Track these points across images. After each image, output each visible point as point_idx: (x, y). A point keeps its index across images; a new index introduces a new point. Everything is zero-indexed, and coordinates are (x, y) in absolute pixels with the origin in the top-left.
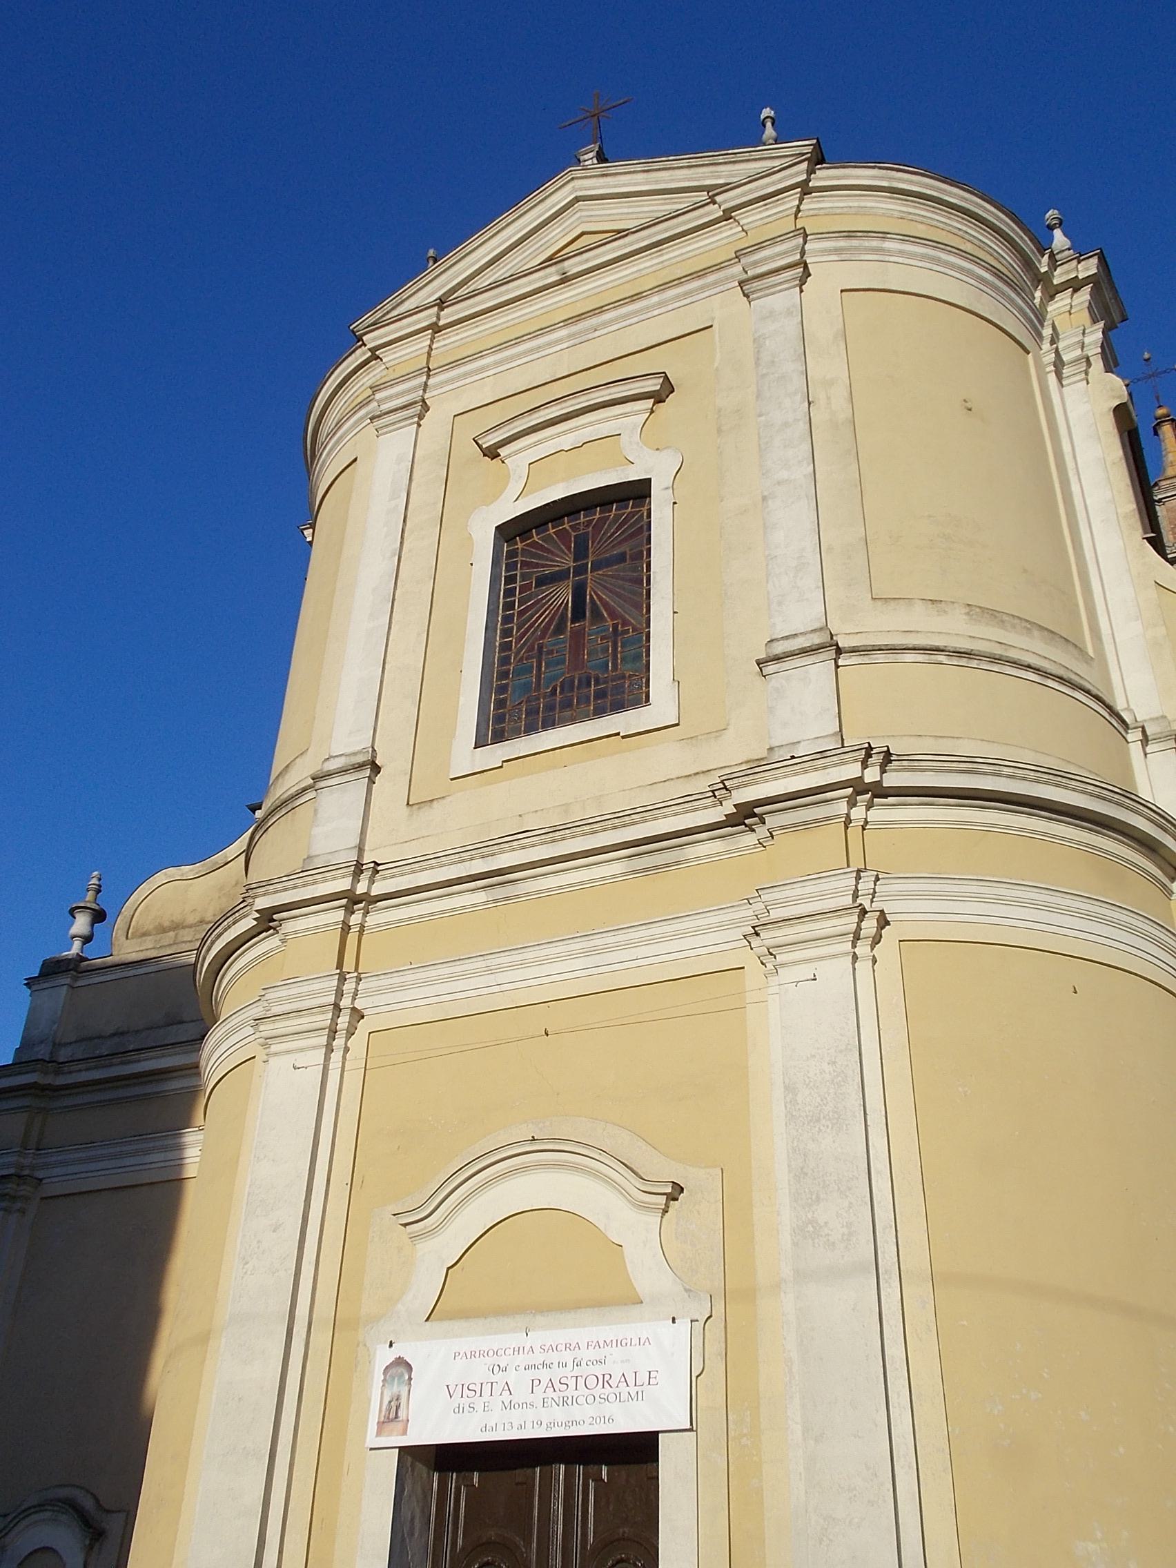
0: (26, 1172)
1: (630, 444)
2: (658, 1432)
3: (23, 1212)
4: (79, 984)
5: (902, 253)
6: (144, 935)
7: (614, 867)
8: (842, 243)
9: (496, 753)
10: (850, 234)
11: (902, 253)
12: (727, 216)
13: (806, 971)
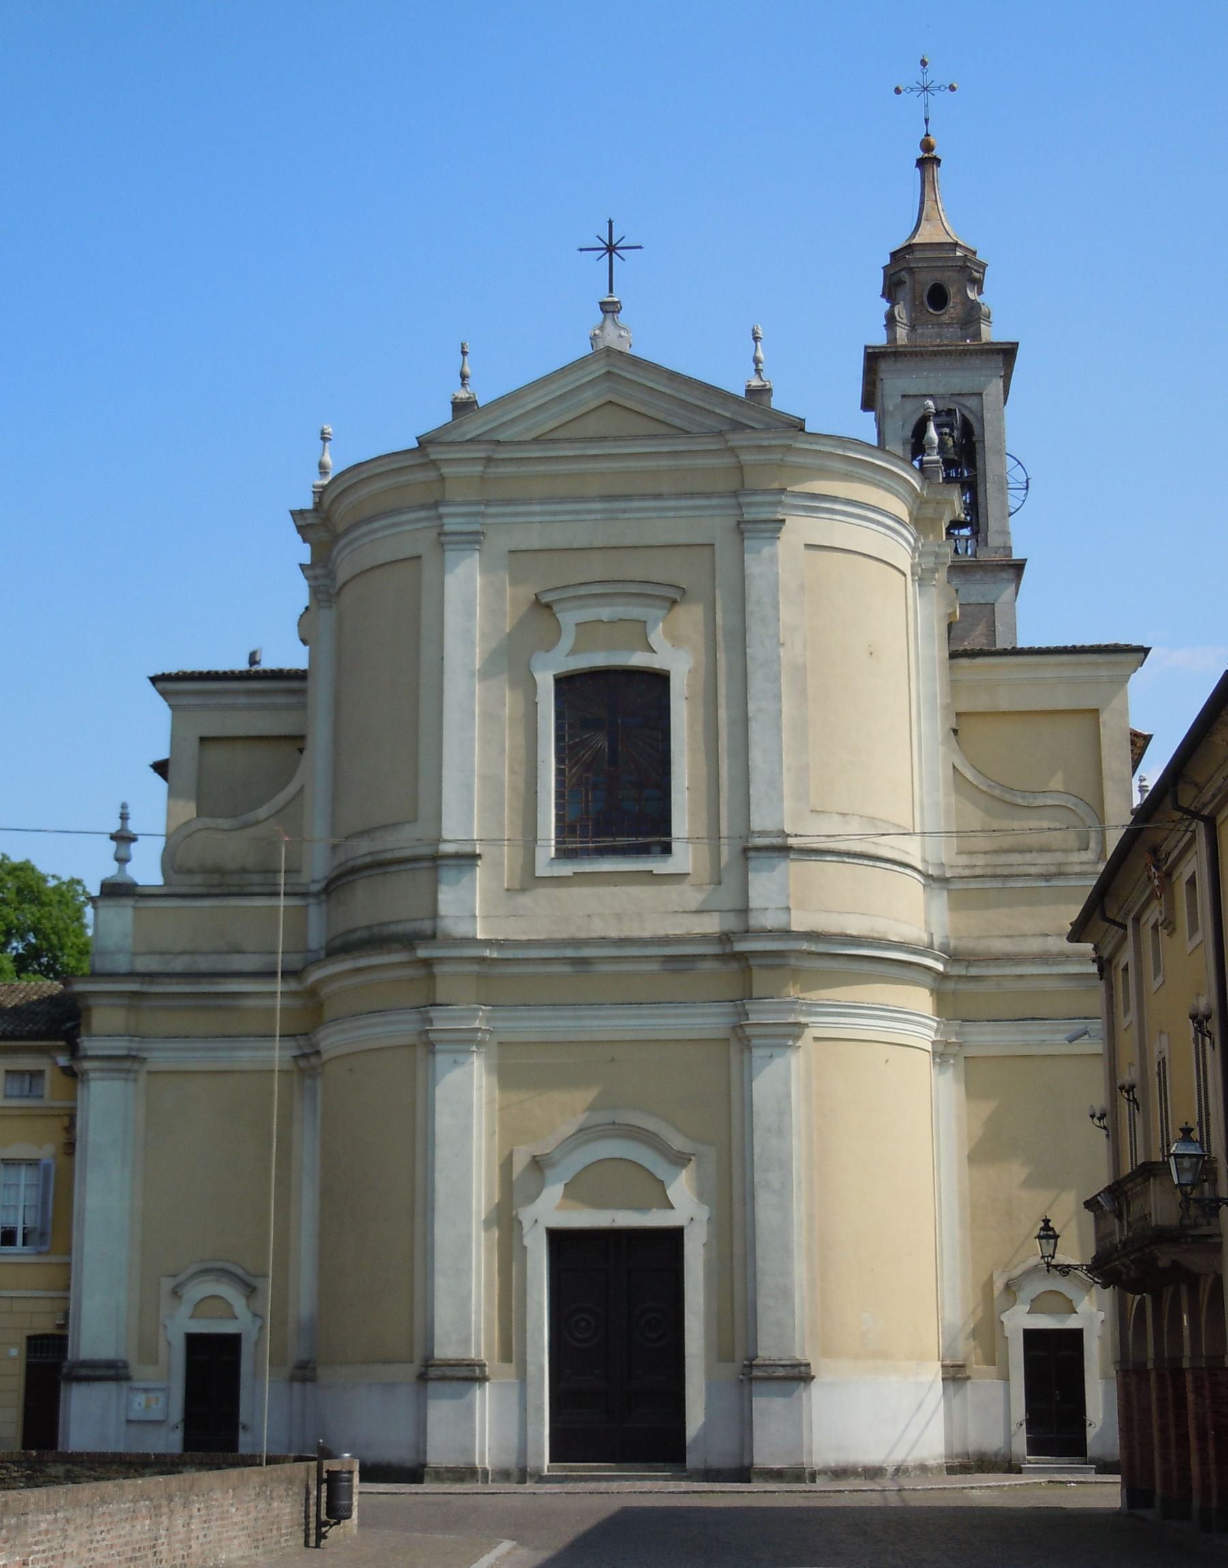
0: (133, 1053)
3: (135, 1080)
9: (567, 869)
13: (767, 1052)
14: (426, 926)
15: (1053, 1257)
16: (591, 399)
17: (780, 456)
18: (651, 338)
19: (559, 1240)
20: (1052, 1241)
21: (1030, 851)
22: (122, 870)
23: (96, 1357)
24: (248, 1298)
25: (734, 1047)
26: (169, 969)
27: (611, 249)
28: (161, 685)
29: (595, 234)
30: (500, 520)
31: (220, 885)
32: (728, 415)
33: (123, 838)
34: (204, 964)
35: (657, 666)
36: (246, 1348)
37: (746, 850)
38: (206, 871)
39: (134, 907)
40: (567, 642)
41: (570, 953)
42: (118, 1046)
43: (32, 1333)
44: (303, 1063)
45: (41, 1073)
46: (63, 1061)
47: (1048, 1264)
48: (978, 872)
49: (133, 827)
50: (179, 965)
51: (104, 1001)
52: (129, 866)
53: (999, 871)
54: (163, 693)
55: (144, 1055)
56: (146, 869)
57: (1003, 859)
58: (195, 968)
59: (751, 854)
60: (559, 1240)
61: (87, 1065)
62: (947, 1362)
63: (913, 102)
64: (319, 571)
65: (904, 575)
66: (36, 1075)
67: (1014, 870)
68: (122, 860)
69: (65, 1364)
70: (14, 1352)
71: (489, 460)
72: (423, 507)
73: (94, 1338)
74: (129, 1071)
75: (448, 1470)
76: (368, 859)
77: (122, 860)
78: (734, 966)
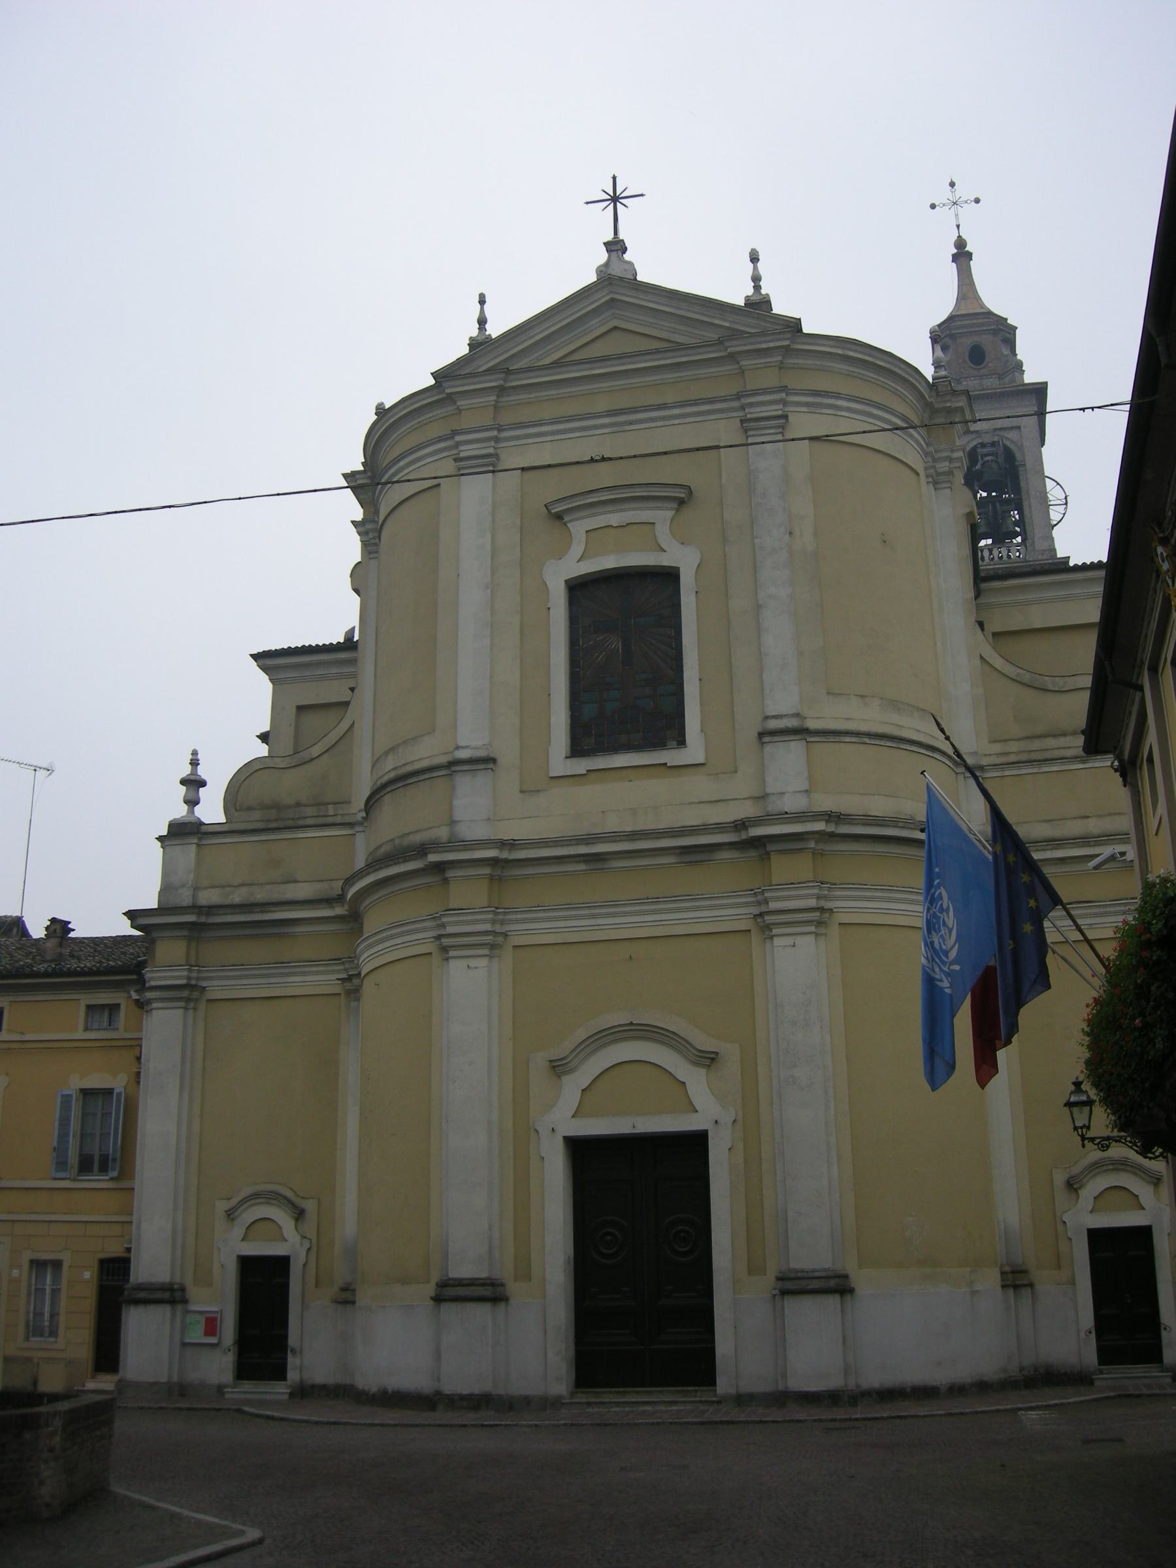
0: (193, 982)
1: (663, 534)
2: (81, 1155)
3: (195, 1009)
4: (204, 842)
5: (849, 410)
6: (250, 809)
7: (671, 859)
8: (810, 399)
9: (581, 766)
10: (816, 393)
11: (849, 410)
12: (732, 357)
13: (788, 941)
14: (443, 833)
15: (1088, 1128)
16: (597, 327)
17: (780, 358)
18: (654, 266)
19: (582, 1151)
20: (1086, 1109)
21: (1064, 735)
22: (191, 811)
23: (153, 1280)
24: (297, 1220)
25: (755, 937)
26: (228, 902)
27: (615, 199)
28: (262, 662)
29: (601, 186)
30: (513, 443)
31: (276, 820)
32: (727, 324)
33: (193, 784)
34: (260, 895)
35: (665, 563)
36: (295, 1270)
37: (761, 735)
38: (265, 807)
39: (198, 845)
40: (577, 549)
41: (583, 850)
42: (178, 977)
43: (103, 1256)
44: (348, 985)
45: (118, 1005)
46: (135, 996)
47: (1083, 1138)
48: (1013, 758)
49: (202, 772)
50: (237, 897)
51: (166, 934)
52: (196, 808)
53: (1034, 756)
54: (265, 669)
55: (204, 984)
56: (211, 810)
57: (1036, 744)
58: (252, 900)
59: (767, 739)
60: (582, 1151)
61: (149, 995)
62: (1007, 1269)
63: (945, 215)
64: (369, 526)
65: (918, 474)
66: (114, 1008)
67: (1048, 755)
68: (192, 802)
69: (126, 1286)
70: (87, 1275)
71: (501, 390)
72: (441, 439)
73: (151, 1264)
74: (188, 1000)
75: (462, 1397)
76: (392, 775)
77: (192, 802)
78: (752, 853)
